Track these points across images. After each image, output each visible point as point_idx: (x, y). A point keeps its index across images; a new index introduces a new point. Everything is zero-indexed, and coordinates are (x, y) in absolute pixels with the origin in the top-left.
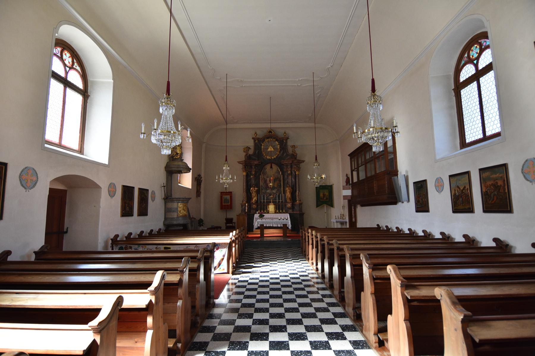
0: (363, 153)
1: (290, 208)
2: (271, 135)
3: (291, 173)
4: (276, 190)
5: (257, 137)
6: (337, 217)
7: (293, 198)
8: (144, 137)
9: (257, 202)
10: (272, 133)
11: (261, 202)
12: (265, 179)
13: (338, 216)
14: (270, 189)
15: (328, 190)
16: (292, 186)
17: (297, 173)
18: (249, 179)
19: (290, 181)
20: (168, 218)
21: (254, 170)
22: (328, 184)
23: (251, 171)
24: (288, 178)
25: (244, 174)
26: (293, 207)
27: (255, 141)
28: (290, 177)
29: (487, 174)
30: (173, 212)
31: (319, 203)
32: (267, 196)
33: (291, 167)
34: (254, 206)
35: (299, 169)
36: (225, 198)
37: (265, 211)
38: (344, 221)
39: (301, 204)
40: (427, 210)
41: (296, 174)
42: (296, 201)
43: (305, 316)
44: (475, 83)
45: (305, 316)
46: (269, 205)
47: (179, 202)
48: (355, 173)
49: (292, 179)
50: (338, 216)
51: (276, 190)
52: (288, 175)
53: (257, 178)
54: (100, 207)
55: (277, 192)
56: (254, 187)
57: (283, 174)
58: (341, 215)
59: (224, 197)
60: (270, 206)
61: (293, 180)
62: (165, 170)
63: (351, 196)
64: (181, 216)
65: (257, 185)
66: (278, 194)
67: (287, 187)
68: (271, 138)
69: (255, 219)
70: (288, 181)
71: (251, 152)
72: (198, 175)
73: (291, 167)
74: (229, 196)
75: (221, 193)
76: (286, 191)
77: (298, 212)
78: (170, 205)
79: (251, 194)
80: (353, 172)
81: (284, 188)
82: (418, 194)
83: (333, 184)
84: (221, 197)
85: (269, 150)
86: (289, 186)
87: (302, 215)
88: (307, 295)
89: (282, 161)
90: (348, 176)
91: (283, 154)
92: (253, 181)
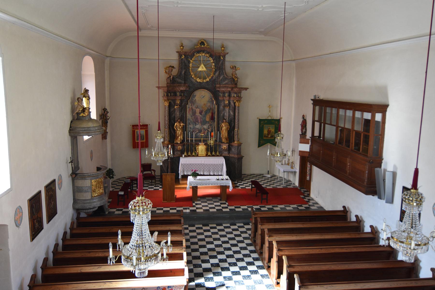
1: (225, 150)
2: (203, 48)
3: (229, 103)
4: (208, 125)
5: (184, 50)
7: (231, 138)
8: (89, 209)
9: (183, 141)
10: (204, 45)
11: (188, 141)
12: (194, 110)
14: (200, 124)
15: (274, 125)
16: (229, 120)
17: (237, 104)
18: (172, 110)
19: (227, 114)
20: (79, 200)
21: (180, 98)
23: (175, 100)
24: (224, 109)
25: (167, 104)
26: (229, 149)
27: (180, 56)
28: (227, 109)
30: (86, 192)
31: (262, 142)
32: (196, 133)
33: (230, 96)
34: (180, 147)
35: (239, 98)
36: (138, 133)
37: (193, 154)
38: (293, 170)
39: (240, 145)
40: (404, 189)
41: (235, 106)
42: (234, 141)
43: (221, 236)
45: (221, 236)
46: (198, 145)
47: (93, 179)
49: (229, 112)
51: (208, 125)
52: (225, 106)
53: (183, 108)
54: (8, 250)
55: (209, 128)
56: (179, 122)
57: (218, 104)
59: (137, 132)
60: (199, 147)
61: (232, 113)
62: (70, 135)
64: (97, 196)
65: (183, 119)
66: (210, 130)
67: (223, 122)
68: (203, 52)
69: (181, 165)
70: (224, 114)
71: (175, 72)
72: (103, 109)
73: (230, 96)
74: (145, 130)
75: (133, 126)
76: (221, 128)
77: (236, 156)
78: (80, 183)
79: (175, 131)
81: (218, 124)
84: (134, 132)
85: (200, 69)
86: (226, 122)
87: (240, 158)
88: (244, 257)
89: (218, 86)
90: (305, 118)
91: (219, 75)
92: (178, 113)
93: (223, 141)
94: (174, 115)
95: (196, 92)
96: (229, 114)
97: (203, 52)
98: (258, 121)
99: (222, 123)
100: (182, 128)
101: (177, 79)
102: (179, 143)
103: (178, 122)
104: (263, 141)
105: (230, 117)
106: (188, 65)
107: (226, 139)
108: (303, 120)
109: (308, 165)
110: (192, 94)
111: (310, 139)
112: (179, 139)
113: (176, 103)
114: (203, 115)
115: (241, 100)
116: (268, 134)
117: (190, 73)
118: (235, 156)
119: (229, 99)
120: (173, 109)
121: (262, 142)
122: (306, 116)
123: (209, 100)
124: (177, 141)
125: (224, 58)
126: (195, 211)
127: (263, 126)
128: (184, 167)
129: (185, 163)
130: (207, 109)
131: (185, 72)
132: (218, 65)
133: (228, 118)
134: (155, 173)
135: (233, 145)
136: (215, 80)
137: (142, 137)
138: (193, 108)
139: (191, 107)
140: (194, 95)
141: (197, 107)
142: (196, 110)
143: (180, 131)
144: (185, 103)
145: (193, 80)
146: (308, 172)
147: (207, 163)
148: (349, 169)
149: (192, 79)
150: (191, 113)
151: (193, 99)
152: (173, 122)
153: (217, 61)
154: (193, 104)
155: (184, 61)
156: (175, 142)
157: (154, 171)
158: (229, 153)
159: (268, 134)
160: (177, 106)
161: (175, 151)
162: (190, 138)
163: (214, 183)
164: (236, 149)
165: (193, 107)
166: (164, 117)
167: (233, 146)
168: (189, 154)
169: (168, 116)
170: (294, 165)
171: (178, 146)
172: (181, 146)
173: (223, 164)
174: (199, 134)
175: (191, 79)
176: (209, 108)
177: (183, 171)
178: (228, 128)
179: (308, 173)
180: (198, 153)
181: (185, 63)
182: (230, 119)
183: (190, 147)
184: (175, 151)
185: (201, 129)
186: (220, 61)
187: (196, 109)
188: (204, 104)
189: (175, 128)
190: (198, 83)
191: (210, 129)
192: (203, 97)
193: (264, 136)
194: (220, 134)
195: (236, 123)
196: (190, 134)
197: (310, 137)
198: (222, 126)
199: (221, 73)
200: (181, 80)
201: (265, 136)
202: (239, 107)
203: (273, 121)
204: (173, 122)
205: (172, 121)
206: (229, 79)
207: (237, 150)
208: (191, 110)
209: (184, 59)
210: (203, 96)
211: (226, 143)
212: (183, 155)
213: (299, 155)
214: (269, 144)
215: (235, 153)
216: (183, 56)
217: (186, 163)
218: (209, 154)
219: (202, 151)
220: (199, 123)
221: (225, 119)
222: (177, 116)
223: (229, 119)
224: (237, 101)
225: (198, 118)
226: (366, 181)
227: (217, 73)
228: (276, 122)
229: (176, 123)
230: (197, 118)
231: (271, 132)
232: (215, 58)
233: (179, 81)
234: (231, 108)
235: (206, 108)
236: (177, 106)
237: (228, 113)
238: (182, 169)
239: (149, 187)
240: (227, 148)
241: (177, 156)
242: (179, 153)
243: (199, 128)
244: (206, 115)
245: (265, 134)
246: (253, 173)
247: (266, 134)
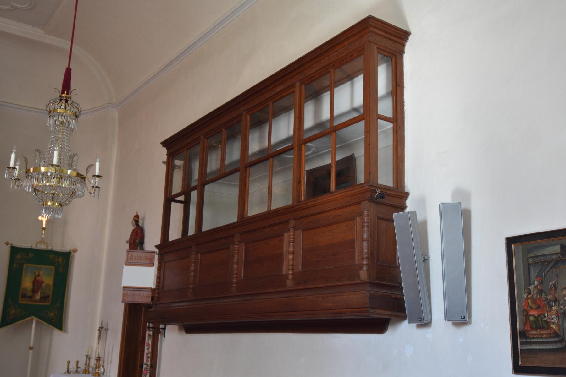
0: (198, 149)
6: (73, 367)
13: (78, 362)
15: (53, 268)
22: (58, 248)
29: (129, 292)
44: (329, 92)
48: (177, 210)
50: (78, 362)
58: (88, 358)
63: (153, 290)
80: (173, 204)
82: (540, 292)
83: (75, 251)
90: (140, 224)
98: (7, 249)
108: (135, 226)
109: (147, 341)
111: (158, 252)
116: (34, 291)
121: (13, 311)
122: (144, 219)
127: (21, 265)
146: (145, 361)
148: (293, 265)
159: (34, 291)
170: (104, 370)
179: (145, 366)
193: (20, 296)
197: (157, 247)
203: (52, 256)
213: (122, 302)
214: (35, 319)
226: (367, 265)
228: (60, 260)
231: (44, 285)
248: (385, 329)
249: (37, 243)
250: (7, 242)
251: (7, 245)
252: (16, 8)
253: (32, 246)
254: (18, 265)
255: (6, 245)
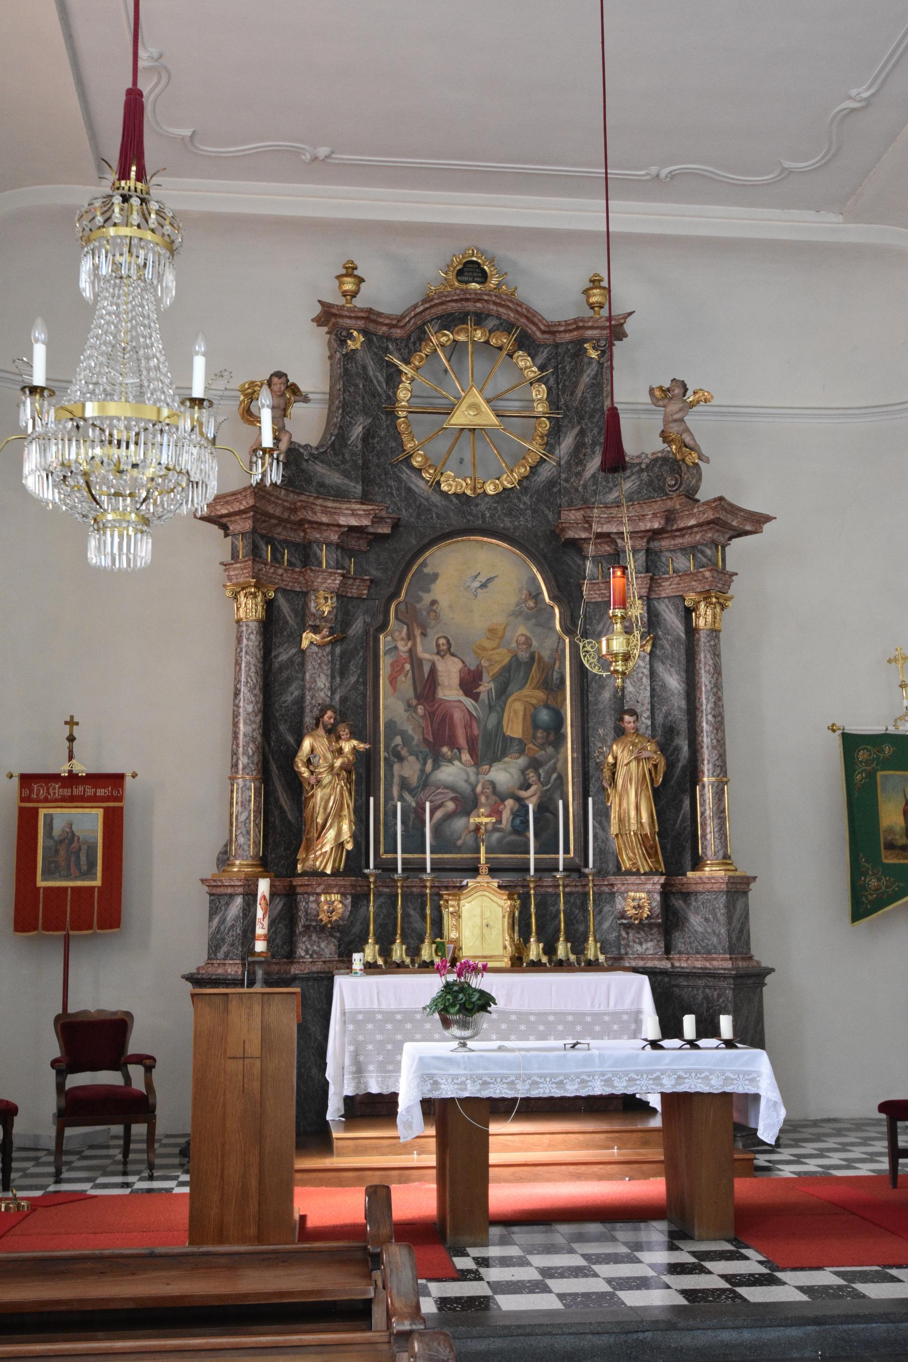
1: (642, 927)
4: (522, 761)
5: (359, 302)
10: (483, 277)
11: (388, 868)
12: (426, 669)
14: (466, 757)
16: (653, 724)
17: (703, 619)
18: (283, 657)
23: (305, 594)
27: (340, 337)
31: (874, 883)
32: (439, 814)
36: (58, 826)
41: (691, 631)
55: (526, 786)
56: (331, 731)
59: (49, 820)
61: (674, 682)
67: (620, 732)
74: (100, 812)
75: (27, 780)
77: (722, 963)
92: (322, 682)
93: (627, 864)
94: (296, 693)
95: (438, 554)
96: (653, 690)
97: (480, 319)
98: (836, 742)
99: (615, 740)
100: (349, 772)
101: (320, 469)
102: (328, 871)
103: (321, 731)
104: (879, 880)
105: (664, 709)
106: (389, 397)
107: (650, 852)
110: (415, 567)
112: (327, 848)
113: (313, 610)
114: (484, 696)
115: (729, 595)
117: (402, 444)
118: (715, 963)
119: (650, 589)
120: (293, 651)
121: (874, 883)
123: (518, 604)
124: (316, 859)
125: (603, 352)
126: (480, 1304)
127: (872, 775)
128: (360, 1038)
129: (368, 1006)
130: (507, 660)
131: (368, 436)
132: (572, 394)
133: (648, 714)
134: (154, 1071)
135: (693, 888)
136: (552, 483)
137: (83, 858)
138: (421, 653)
139: (406, 649)
140: (426, 570)
141: (446, 650)
142: (441, 666)
143: (334, 788)
144: (368, 619)
145: (420, 486)
147: (525, 1008)
149: (414, 478)
150: (406, 684)
151: (420, 599)
152: (291, 739)
153: (564, 373)
154: (417, 632)
155: (364, 368)
156: (299, 866)
157: (147, 1062)
158: (668, 950)
160: (315, 633)
161: (303, 934)
162: (403, 852)
163: (626, 1073)
164: (721, 912)
165: (419, 648)
166: (232, 696)
167: (696, 893)
168: (398, 952)
169: (257, 691)
171: (319, 894)
172: (343, 895)
173: (639, 1012)
174: (459, 824)
175: (406, 475)
176: (524, 656)
177: (354, 1069)
178: (655, 766)
180: (461, 949)
181: (367, 379)
182: (660, 719)
183: (405, 915)
184: (300, 928)
185: (474, 789)
186: (578, 371)
187: (436, 658)
188: (492, 631)
189: (303, 769)
190: (451, 501)
191: (533, 788)
192: (484, 586)
194: (600, 823)
195: (706, 740)
196: (403, 822)
198: (615, 758)
199: (588, 440)
200: (346, 474)
201: (890, 846)
202: (717, 637)
204: (291, 739)
205: (282, 728)
206: (643, 466)
207: (722, 919)
208: (408, 667)
209: (359, 356)
210: (482, 579)
211: (645, 874)
212: (357, 965)
215: (715, 940)
216: (355, 334)
217: (376, 1006)
218: (535, 950)
219: (483, 937)
220: (459, 750)
221: (632, 713)
222: (313, 697)
223: (652, 717)
224: (706, 596)
225: (452, 718)
227: (567, 443)
229: (312, 735)
230: (443, 719)
232: (549, 359)
233: (327, 482)
234: (667, 646)
235: (502, 657)
236: (316, 630)
237: (646, 681)
238: (352, 1048)
239: (101, 1180)
240: (658, 910)
241: (314, 969)
242: (328, 949)
243: (463, 785)
244: (503, 697)
245: (890, 830)
246: (825, 1117)
247: (898, 829)
248: (80, 1019)
249: (896, 720)
250: (833, 725)
251: (834, 731)
252: (791, 172)
253: (887, 729)
254: (864, 775)
255: (830, 731)
